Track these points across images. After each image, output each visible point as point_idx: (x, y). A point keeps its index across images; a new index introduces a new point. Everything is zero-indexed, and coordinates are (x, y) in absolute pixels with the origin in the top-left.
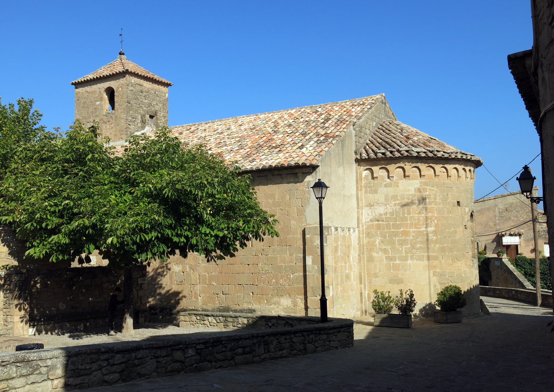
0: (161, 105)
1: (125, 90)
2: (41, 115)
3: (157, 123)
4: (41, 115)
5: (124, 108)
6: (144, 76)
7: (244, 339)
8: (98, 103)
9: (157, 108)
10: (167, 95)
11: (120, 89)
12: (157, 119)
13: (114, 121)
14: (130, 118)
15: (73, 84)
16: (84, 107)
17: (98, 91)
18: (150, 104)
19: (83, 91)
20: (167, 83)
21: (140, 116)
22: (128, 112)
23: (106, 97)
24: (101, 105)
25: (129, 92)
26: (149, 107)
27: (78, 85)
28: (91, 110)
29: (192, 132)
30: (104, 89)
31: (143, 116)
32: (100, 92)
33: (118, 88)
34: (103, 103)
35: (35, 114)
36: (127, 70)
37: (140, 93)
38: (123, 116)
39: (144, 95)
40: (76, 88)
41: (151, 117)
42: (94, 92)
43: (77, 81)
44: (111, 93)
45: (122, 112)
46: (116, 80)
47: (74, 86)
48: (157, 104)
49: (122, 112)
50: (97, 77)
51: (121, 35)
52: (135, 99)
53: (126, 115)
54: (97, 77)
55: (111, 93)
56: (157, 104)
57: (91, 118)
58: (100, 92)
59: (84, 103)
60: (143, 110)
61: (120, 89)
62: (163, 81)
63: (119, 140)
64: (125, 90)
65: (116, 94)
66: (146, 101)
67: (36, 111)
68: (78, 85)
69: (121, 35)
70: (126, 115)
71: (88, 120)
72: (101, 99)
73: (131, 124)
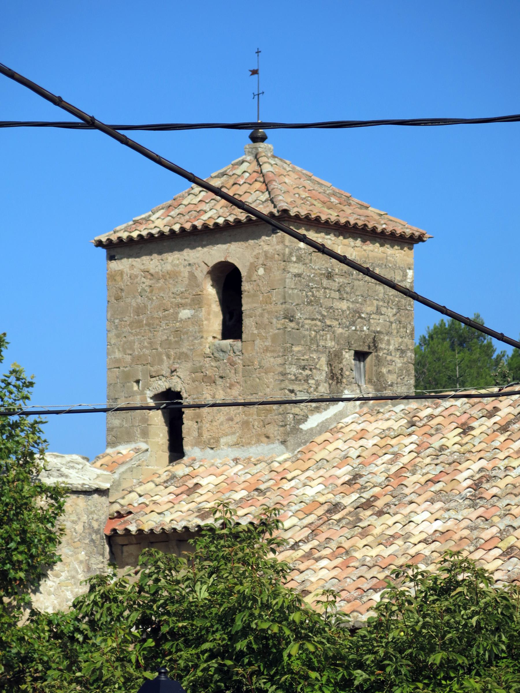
0: (390, 312)
1: (277, 274)
2: (31, 384)
3: (380, 375)
4: (31, 384)
5: (274, 338)
6: (337, 223)
7: (229, 435)
8: (185, 313)
9: (378, 323)
10: (410, 273)
11: (261, 271)
12: (379, 361)
13: (239, 377)
14: (294, 370)
15: (99, 244)
16: (139, 324)
17: (185, 272)
18: (357, 312)
19: (136, 271)
20: (412, 236)
21: (324, 360)
22: (287, 351)
23: (211, 292)
24: (195, 321)
25: (290, 282)
26: (353, 323)
27: (116, 249)
28: (161, 336)
29: (504, 429)
30: (206, 269)
31: (334, 357)
32: (192, 276)
33: (253, 268)
34: (203, 314)
35: (12, 379)
36: (285, 212)
37: (325, 282)
38: (271, 361)
39: (335, 286)
40: (111, 258)
41: (360, 356)
42: (173, 275)
43: (114, 238)
44: (228, 280)
45: (266, 350)
46: (245, 239)
47: (103, 252)
48: (378, 312)
49: (266, 350)
50: (182, 229)
51: (255, 72)
52: (310, 303)
53: (280, 361)
54: (182, 229)
55: (228, 280)
56: (378, 312)
57: (161, 362)
58: (192, 276)
59: (139, 310)
60: (333, 339)
61: (261, 271)
62: (399, 231)
63: (259, 441)
64: (277, 274)
65: (245, 286)
66: (344, 305)
67: (14, 371)
68: (116, 249)
69: (255, 72)
70: (280, 361)
71: (153, 370)
72: (197, 301)
73: (296, 388)
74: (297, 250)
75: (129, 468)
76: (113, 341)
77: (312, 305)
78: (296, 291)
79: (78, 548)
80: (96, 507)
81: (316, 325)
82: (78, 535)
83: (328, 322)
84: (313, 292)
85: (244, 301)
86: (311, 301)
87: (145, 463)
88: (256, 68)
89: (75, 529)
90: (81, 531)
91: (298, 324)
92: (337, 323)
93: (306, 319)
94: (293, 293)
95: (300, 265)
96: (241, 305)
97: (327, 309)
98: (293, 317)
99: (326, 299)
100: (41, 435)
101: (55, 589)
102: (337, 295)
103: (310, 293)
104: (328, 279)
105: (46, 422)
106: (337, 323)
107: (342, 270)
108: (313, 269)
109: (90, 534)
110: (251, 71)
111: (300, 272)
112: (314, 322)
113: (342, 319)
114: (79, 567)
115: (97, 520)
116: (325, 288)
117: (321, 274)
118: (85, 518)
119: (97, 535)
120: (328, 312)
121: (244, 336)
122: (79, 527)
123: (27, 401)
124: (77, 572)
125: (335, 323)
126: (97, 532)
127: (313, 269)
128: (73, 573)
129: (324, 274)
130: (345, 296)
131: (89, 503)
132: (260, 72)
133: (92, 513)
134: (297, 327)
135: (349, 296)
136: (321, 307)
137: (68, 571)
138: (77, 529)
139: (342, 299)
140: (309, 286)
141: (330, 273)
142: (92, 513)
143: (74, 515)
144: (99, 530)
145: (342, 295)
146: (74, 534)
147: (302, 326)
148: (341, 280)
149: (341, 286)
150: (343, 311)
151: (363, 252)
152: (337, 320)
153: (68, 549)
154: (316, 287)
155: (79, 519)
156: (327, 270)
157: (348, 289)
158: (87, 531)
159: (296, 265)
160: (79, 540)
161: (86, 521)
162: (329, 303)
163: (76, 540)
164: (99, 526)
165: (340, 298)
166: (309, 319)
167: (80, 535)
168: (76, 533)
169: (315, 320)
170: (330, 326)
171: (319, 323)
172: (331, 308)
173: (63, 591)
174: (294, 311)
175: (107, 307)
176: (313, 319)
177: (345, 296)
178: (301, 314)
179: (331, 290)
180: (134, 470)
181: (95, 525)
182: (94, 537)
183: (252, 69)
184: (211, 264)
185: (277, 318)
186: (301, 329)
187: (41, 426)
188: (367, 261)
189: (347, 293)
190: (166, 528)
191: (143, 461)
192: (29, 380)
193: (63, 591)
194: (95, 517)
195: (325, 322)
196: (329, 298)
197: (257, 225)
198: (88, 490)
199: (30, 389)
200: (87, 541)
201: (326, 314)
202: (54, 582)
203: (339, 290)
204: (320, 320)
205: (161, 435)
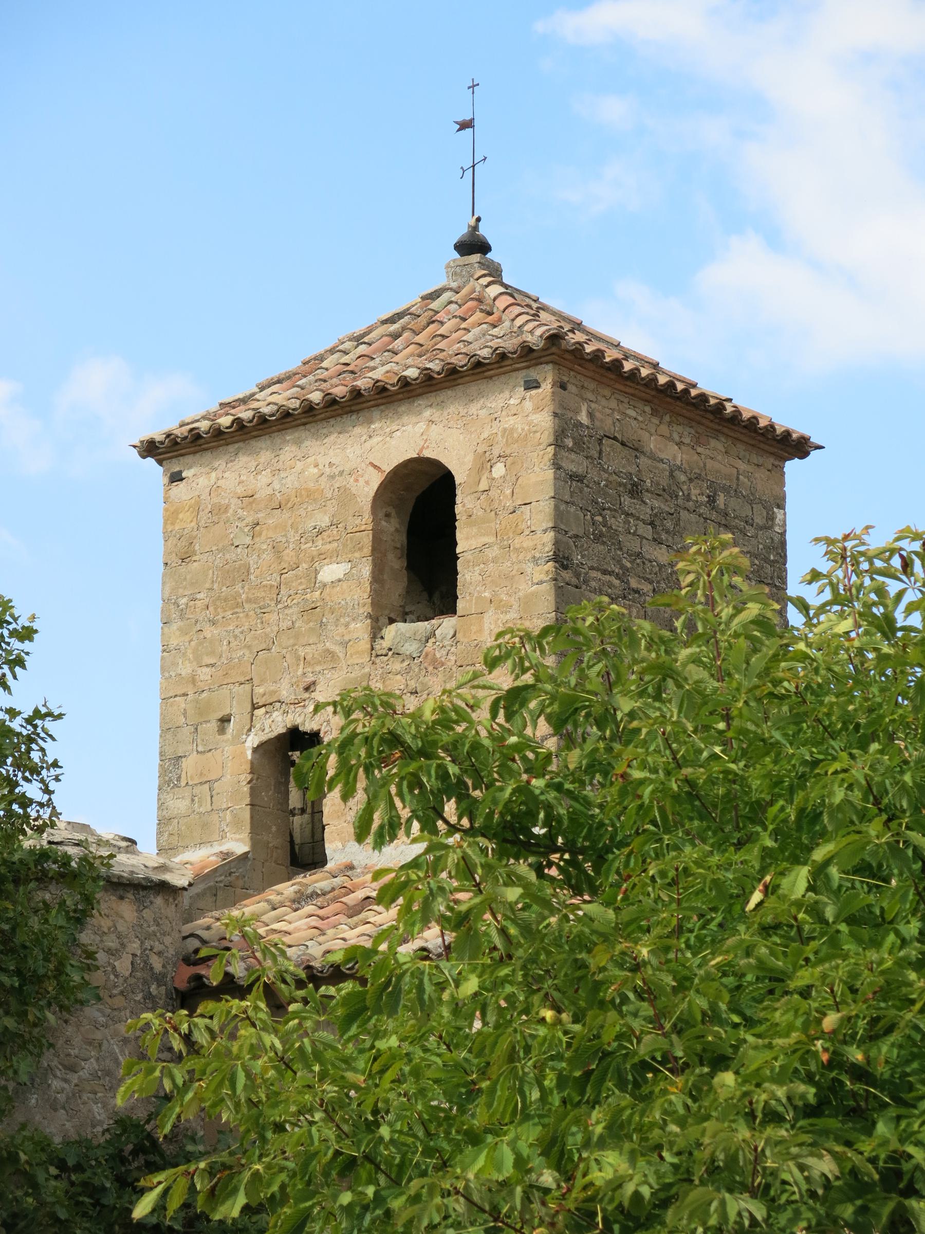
37: (627, 500)
39: (645, 512)
51: (465, 125)
69: (465, 125)
74: (575, 425)
75: (210, 888)
76: (174, 642)
77: (604, 543)
78: (572, 509)
79: (119, 1009)
80: (158, 925)
81: (611, 585)
82: (121, 980)
83: (634, 583)
84: (604, 517)
85: (459, 536)
86: (601, 535)
87: (240, 883)
88: (468, 118)
89: (114, 967)
90: (127, 974)
91: (577, 575)
92: (650, 587)
93: (592, 568)
94: (568, 512)
95: (580, 458)
96: (455, 544)
97: (631, 555)
98: (568, 559)
99: (630, 536)
100: (48, 745)
101: (68, 1098)
102: (647, 532)
103: (599, 518)
104: (632, 497)
105: (60, 716)
106: (650, 587)
107: (658, 484)
108: (604, 470)
109: (145, 982)
110: (456, 123)
111: (581, 470)
112: (608, 577)
113: (658, 582)
114: (122, 1051)
115: (160, 954)
116: (627, 515)
117: (620, 484)
118: (135, 946)
119: (159, 986)
120: (632, 562)
121: (460, 605)
122: (123, 965)
123: (18, 669)
124: (117, 1062)
125: (646, 587)
126: (160, 979)
127: (604, 470)
128: (108, 1063)
129: (625, 485)
130: (664, 536)
131: (147, 913)
132: (476, 123)
133: (148, 936)
134: (574, 581)
135: (670, 539)
136: (621, 549)
137: (97, 1060)
138: (118, 969)
139: (658, 541)
140: (597, 503)
141: (635, 485)
142: (148, 936)
143: (113, 936)
144: (164, 975)
145: (658, 533)
146: (112, 977)
147: (586, 582)
148: (656, 504)
149: (656, 515)
150: (661, 567)
151: (696, 457)
152: (651, 582)
153: (99, 1010)
154: (609, 509)
155: (123, 945)
156: (631, 479)
157: (669, 524)
158: (139, 974)
159: (573, 456)
160: (122, 993)
161: (138, 953)
162: (633, 545)
163: (115, 992)
164: (164, 966)
165: (655, 540)
166: (597, 569)
167: (125, 981)
168: (117, 976)
169: (610, 573)
170: (637, 591)
171: (617, 582)
172: (639, 555)
173: (84, 1103)
174: (569, 548)
175: (164, 575)
176: (605, 572)
177: (664, 536)
178: (583, 557)
179: (638, 519)
180: (220, 893)
181: (157, 964)
182: (153, 988)
183: (460, 119)
184: (388, 468)
185: (535, 560)
186: (584, 587)
187: (49, 724)
188: (703, 474)
189: (668, 532)
190: (316, 964)
191: (237, 877)
192: (23, 621)
193: (84, 1103)
194: (158, 947)
195: (628, 583)
196: (634, 534)
197: (491, 377)
198: (144, 883)
199: (27, 646)
200: (139, 997)
201: (629, 565)
202: (66, 1081)
203: (652, 524)
204: (617, 576)
205: (274, 829)
